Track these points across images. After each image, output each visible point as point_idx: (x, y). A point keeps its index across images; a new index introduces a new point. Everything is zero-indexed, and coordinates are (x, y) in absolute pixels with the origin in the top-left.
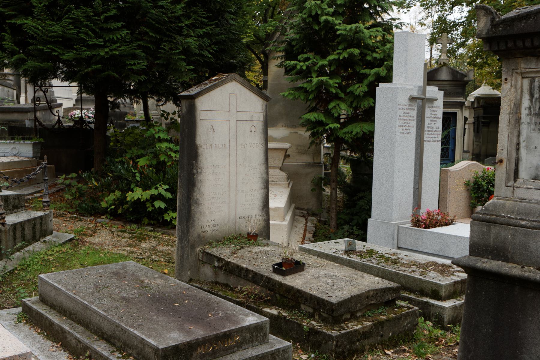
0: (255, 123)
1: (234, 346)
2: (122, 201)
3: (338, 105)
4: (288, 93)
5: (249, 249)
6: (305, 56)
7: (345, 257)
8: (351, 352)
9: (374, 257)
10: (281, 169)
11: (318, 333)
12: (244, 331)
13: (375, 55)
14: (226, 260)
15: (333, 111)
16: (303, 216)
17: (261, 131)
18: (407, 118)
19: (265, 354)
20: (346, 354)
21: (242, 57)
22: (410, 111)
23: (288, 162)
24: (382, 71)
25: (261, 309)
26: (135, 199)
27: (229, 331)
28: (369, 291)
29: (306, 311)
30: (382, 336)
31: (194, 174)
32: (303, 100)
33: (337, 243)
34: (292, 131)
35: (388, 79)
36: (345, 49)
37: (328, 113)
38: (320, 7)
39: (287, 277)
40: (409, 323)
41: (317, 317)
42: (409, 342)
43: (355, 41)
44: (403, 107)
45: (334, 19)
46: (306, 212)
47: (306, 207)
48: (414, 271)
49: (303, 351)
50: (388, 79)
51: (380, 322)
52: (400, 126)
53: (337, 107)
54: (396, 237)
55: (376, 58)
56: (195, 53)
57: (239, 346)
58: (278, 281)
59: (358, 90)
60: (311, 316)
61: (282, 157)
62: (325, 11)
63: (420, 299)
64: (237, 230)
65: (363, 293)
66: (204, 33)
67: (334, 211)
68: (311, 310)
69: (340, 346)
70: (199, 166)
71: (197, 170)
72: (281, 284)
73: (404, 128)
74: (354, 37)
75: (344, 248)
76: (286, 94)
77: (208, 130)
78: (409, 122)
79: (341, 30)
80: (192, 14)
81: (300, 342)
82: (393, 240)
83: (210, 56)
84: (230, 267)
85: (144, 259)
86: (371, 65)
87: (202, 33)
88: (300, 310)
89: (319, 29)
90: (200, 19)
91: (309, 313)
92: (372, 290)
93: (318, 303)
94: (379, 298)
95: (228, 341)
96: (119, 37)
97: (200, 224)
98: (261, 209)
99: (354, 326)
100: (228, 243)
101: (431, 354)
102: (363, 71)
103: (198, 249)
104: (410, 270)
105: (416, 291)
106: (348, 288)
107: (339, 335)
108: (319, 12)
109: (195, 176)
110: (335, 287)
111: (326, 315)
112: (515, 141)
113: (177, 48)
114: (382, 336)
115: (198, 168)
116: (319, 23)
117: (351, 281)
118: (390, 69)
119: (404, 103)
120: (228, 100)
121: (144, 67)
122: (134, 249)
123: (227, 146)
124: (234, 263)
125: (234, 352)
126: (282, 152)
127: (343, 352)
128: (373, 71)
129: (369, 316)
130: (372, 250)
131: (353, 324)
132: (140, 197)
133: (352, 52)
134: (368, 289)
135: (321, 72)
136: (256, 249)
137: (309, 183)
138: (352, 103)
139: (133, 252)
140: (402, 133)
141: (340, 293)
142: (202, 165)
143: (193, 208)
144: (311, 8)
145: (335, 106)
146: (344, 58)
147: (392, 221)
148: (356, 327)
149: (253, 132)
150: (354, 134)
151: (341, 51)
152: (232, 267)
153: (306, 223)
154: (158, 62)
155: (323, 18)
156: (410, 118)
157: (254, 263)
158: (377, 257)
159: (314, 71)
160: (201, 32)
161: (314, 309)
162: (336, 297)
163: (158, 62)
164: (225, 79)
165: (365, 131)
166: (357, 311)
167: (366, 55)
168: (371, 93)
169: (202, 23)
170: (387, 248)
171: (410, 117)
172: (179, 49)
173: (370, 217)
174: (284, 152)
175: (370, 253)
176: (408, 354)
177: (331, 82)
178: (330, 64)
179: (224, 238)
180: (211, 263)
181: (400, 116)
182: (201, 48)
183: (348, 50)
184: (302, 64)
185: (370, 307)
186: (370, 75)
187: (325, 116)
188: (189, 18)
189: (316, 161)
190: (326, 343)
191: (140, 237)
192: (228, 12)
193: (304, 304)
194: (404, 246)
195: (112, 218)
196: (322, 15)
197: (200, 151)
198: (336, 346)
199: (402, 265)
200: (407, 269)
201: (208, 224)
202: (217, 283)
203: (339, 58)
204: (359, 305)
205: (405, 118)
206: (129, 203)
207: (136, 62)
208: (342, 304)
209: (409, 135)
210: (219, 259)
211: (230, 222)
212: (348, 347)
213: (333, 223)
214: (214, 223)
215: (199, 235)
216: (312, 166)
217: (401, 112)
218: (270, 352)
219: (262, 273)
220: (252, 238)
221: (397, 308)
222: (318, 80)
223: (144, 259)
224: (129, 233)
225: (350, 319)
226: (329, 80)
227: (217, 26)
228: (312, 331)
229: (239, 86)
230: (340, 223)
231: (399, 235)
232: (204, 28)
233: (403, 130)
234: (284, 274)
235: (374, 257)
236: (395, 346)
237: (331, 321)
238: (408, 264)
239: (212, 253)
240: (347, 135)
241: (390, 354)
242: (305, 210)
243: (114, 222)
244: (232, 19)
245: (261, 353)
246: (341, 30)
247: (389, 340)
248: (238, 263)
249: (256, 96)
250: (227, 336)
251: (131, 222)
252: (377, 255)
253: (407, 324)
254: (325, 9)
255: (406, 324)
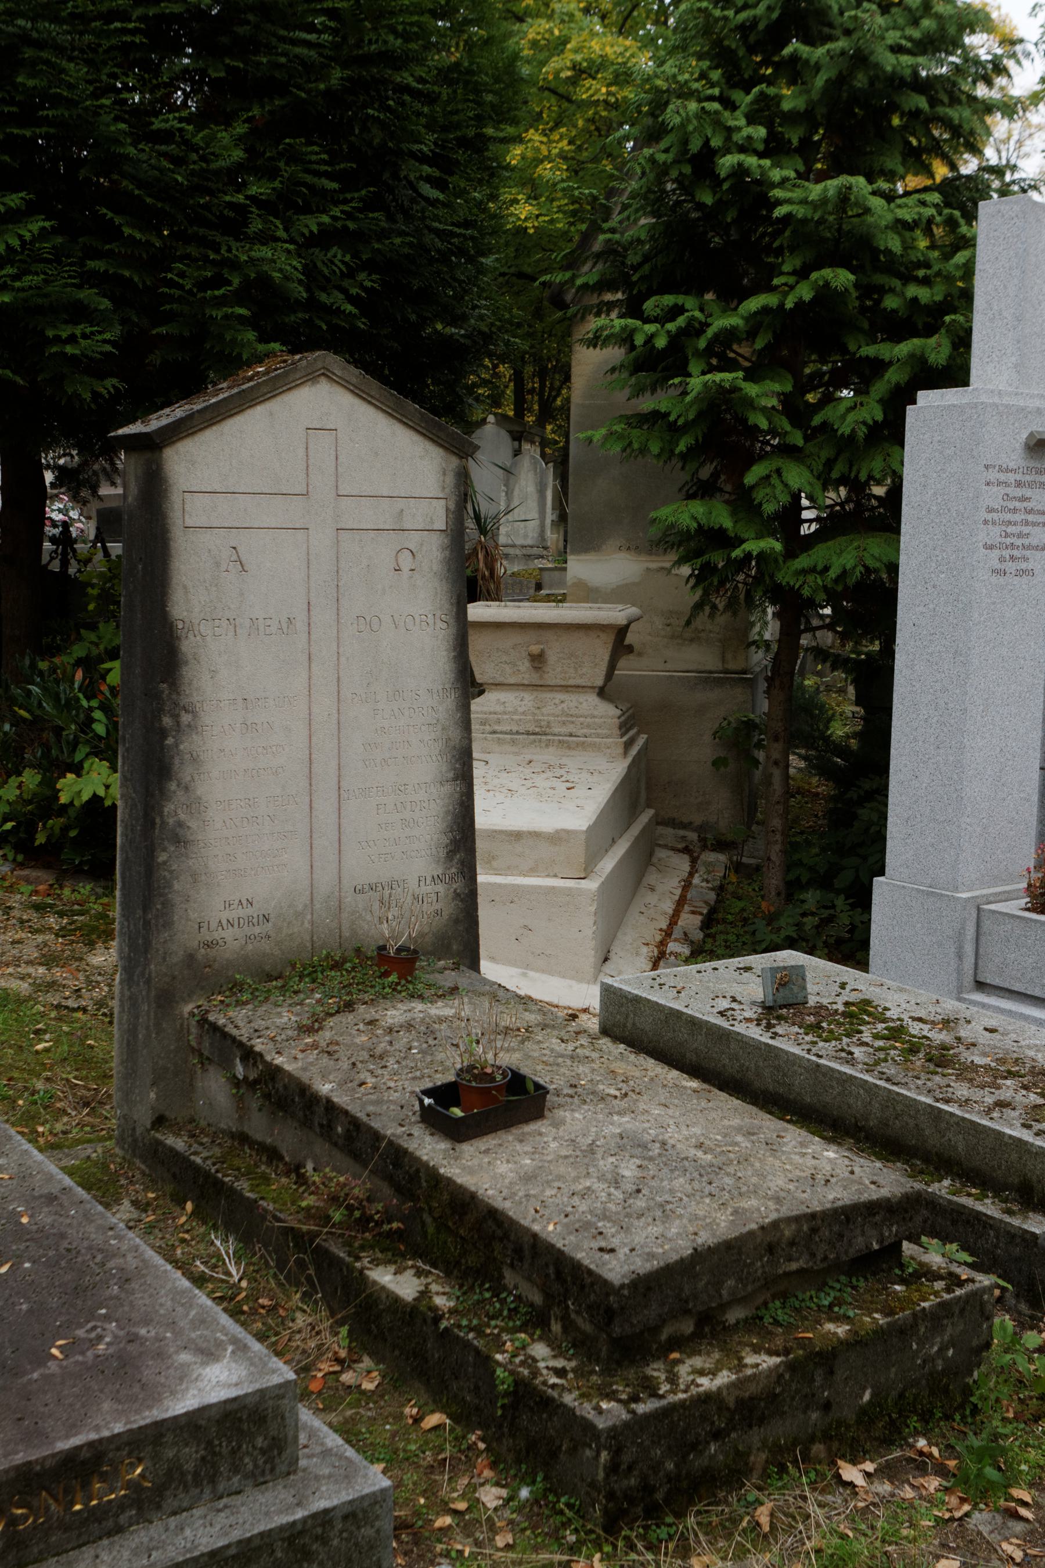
0: (413, 540)
1: (122, 1505)
2: (46, 803)
3: (779, 472)
4: (603, 431)
5: (371, 1013)
6: (668, 300)
7: (755, 1033)
8: (685, 1484)
9: (867, 1037)
10: (602, 693)
11: (547, 1404)
12: (169, 1438)
13: (913, 291)
14: (268, 1058)
15: (759, 495)
16: (686, 850)
17: (436, 567)
18: (1018, 517)
19: (257, 1542)
20: (659, 1496)
21: (481, 318)
22: (1028, 493)
23: (626, 668)
24: (937, 349)
25: (361, 1272)
26: (85, 797)
27: (91, 1444)
28: (775, 1224)
29: (518, 1298)
30: (827, 1406)
31: (163, 734)
32: (659, 456)
33: (747, 969)
34: (654, 566)
35: (955, 374)
36: (802, 274)
37: (744, 502)
38: (717, 123)
39: (467, 1148)
40: (952, 1343)
41: (556, 1327)
42: (948, 1417)
43: (842, 240)
44: (1002, 477)
45: (767, 163)
46: (693, 836)
47: (698, 819)
48: (1001, 1104)
49: (493, 1465)
50: (955, 374)
51: (819, 1354)
52: (991, 547)
53: (775, 480)
54: (969, 949)
55: (915, 300)
56: (297, 300)
57: (145, 1503)
58: (426, 1164)
59: (851, 418)
60: (536, 1322)
61: (604, 654)
62: (738, 138)
63: (1016, 1222)
64: (346, 934)
65: (751, 1233)
66: (323, 230)
67: (778, 837)
68: (537, 1298)
69: (630, 1468)
70: (184, 701)
71: (176, 717)
72: (437, 1181)
73: (1006, 553)
74: (839, 230)
75: (760, 996)
76: (599, 434)
77: (218, 564)
78: (1026, 530)
79: (789, 201)
80: (282, 164)
81: (483, 1425)
82: (960, 956)
83: (349, 308)
84: (279, 1086)
85: (84, 1010)
86: (898, 328)
87: (315, 229)
88: (498, 1288)
89: (719, 203)
90: (309, 179)
91: (532, 1305)
92: (789, 1220)
93: (558, 1273)
94: (824, 1246)
95: (86, 1485)
96: (15, 243)
97: (193, 915)
98: (443, 853)
99: (702, 1376)
100: (306, 984)
101: (1031, 1485)
102: (869, 351)
103: (188, 1008)
104: (989, 1100)
105: (1006, 1187)
106: (693, 1207)
107: (626, 1425)
108: (716, 142)
109: (170, 741)
110: (640, 1203)
111: (588, 1328)
112: (992, 899)
113: (219, 281)
114: (827, 1406)
115: (177, 709)
116: (716, 182)
117: (709, 1173)
118: (963, 341)
119: (1004, 460)
120: (301, 452)
121: (108, 348)
122: (58, 973)
123: (300, 625)
124: (290, 1075)
125: (119, 1530)
126: (603, 636)
127: (647, 1489)
128: (904, 349)
129: (776, 1323)
130: (867, 1002)
131: (698, 1362)
132: (101, 792)
133: (827, 284)
134: (774, 1216)
135: (719, 354)
136: (394, 1014)
137: (707, 738)
138: (829, 464)
139: (52, 986)
140: (995, 572)
141: (655, 1230)
142: (195, 698)
143: (162, 857)
144: (683, 125)
145: (768, 477)
146: (800, 304)
147: (956, 889)
148: (705, 1383)
149: (405, 569)
150: (833, 574)
151: (791, 280)
152: (285, 1087)
153: (691, 874)
154: (163, 330)
155: (728, 162)
156: (1030, 518)
157: (362, 1076)
158: (876, 1037)
159: (698, 354)
160: (311, 224)
161: (548, 1296)
162: (625, 1252)
163: (163, 330)
164: (286, 374)
165: (870, 563)
166: (724, 1307)
167: (883, 291)
168: (891, 431)
169: (324, 193)
170: (925, 996)
171: (1030, 511)
172: (229, 283)
173: (882, 872)
174: (609, 638)
175: (859, 1013)
176: (933, 1483)
177: (752, 389)
178: (757, 322)
179: (293, 966)
180: (226, 1064)
181: (990, 510)
182: (312, 276)
183: (814, 275)
184: (650, 328)
185: (781, 1288)
186: (891, 363)
187: (734, 513)
188: (272, 174)
189: (731, 666)
190: (574, 1450)
191: (93, 929)
192: (413, 155)
193: (512, 1266)
194: (997, 982)
195: (20, 858)
196: (728, 151)
197: (186, 646)
198: (613, 1468)
199: (967, 1072)
200: (977, 1094)
201: (225, 916)
202: (243, 1138)
203: (781, 305)
204: (731, 1283)
205: (1009, 517)
206: (72, 812)
207: (78, 332)
208: (646, 1285)
209: (1025, 579)
210: (249, 1055)
211: (317, 906)
212: (670, 1466)
213: (774, 880)
214: (250, 911)
215: (191, 958)
216: (719, 682)
217: (993, 496)
218: (282, 1528)
219: (376, 1124)
220: (396, 967)
221: (903, 1281)
222: (705, 384)
223: (84, 1010)
224: (61, 914)
225: (694, 1335)
226: (744, 385)
227: (370, 205)
228: (527, 1396)
229: (346, 400)
230: (798, 879)
231: (983, 939)
232: (324, 211)
233: (1002, 560)
234: (457, 1133)
235: (867, 1037)
236: (887, 1442)
237: (604, 1353)
238: (987, 1068)
239: (230, 1029)
240: (810, 578)
241: (860, 1481)
242: (694, 830)
243: (26, 872)
244: (429, 179)
245: (236, 1535)
246: (789, 201)
247: (859, 1422)
248: (305, 1077)
249: (416, 437)
250: (82, 1467)
251: (78, 873)
252: (880, 1026)
253: (942, 1349)
254: (739, 129)
255: (936, 1349)
